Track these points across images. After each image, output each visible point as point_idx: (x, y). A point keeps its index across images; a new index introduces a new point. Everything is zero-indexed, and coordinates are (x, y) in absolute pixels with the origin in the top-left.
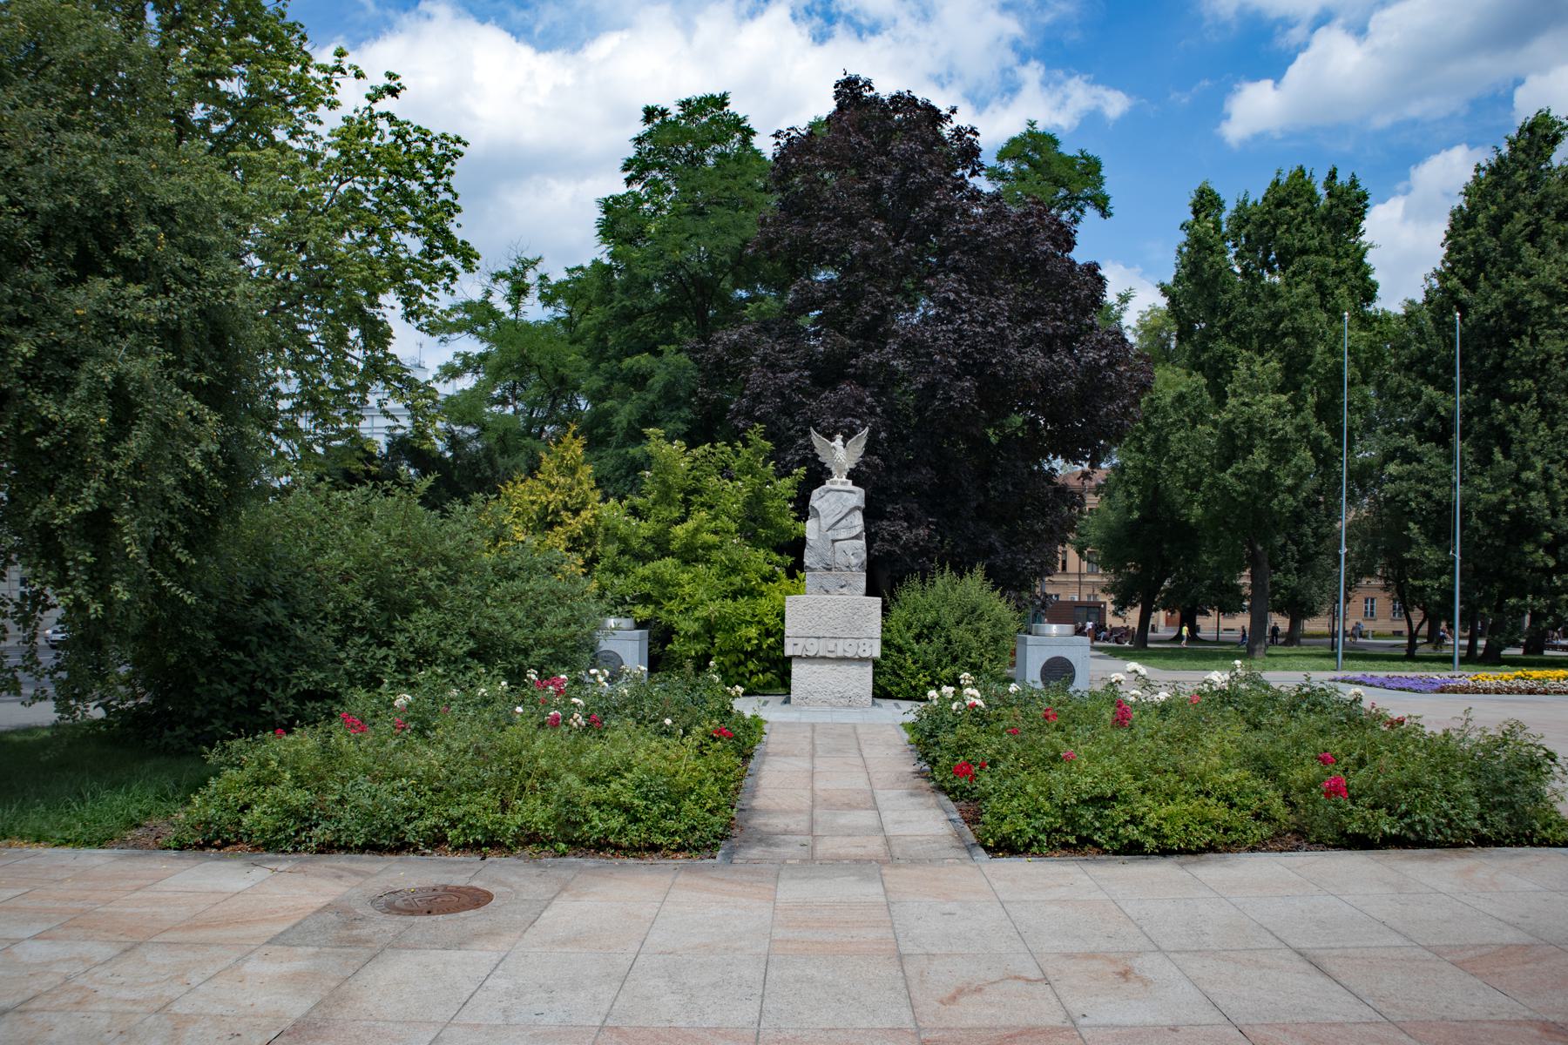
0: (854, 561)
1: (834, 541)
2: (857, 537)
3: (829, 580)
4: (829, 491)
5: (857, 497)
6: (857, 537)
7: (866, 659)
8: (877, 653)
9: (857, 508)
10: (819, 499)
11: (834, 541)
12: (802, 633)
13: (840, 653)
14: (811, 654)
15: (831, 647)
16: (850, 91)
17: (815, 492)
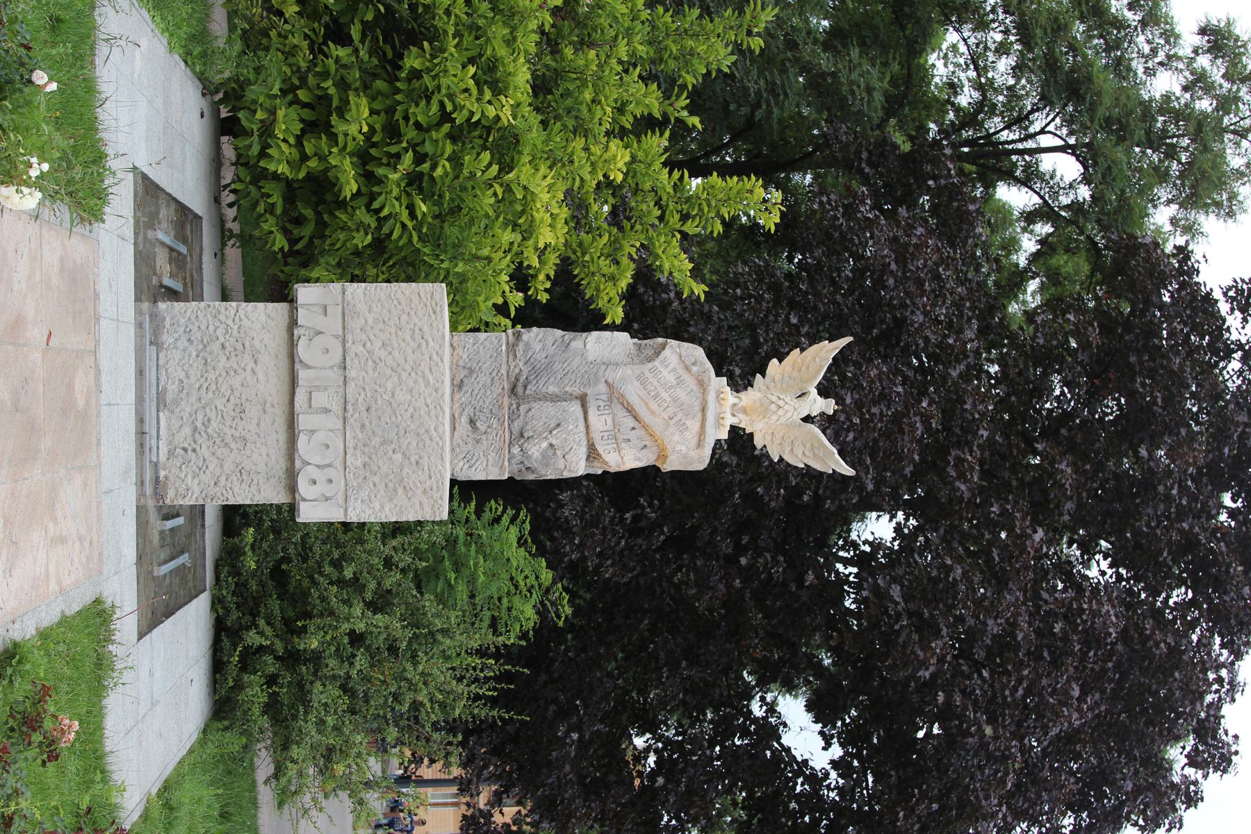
0: (536, 450)
1: (583, 400)
2: (592, 454)
3: (489, 392)
4: (702, 384)
5: (688, 452)
6: (592, 454)
7: (292, 488)
8: (309, 513)
9: (663, 457)
10: (682, 359)
11: (583, 400)
12: (355, 324)
13: (304, 421)
14: (302, 350)
15: (320, 399)
16: (739, 440)
17: (698, 352)
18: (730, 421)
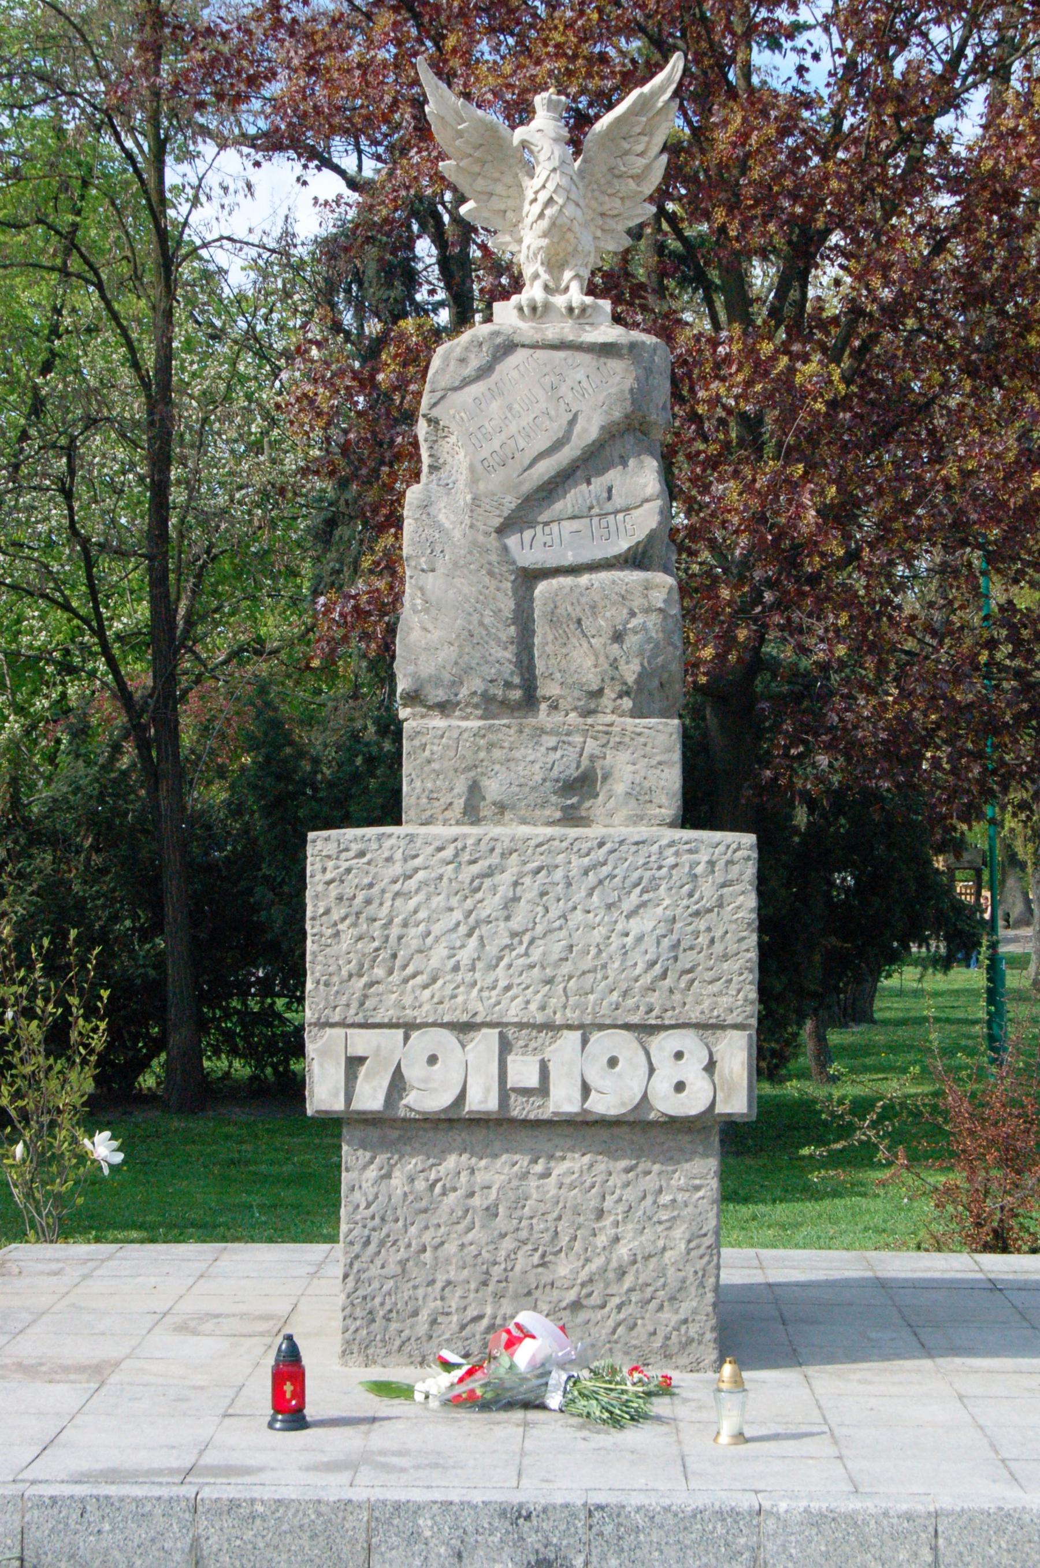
2: (637, 559)
18: (576, 295)
